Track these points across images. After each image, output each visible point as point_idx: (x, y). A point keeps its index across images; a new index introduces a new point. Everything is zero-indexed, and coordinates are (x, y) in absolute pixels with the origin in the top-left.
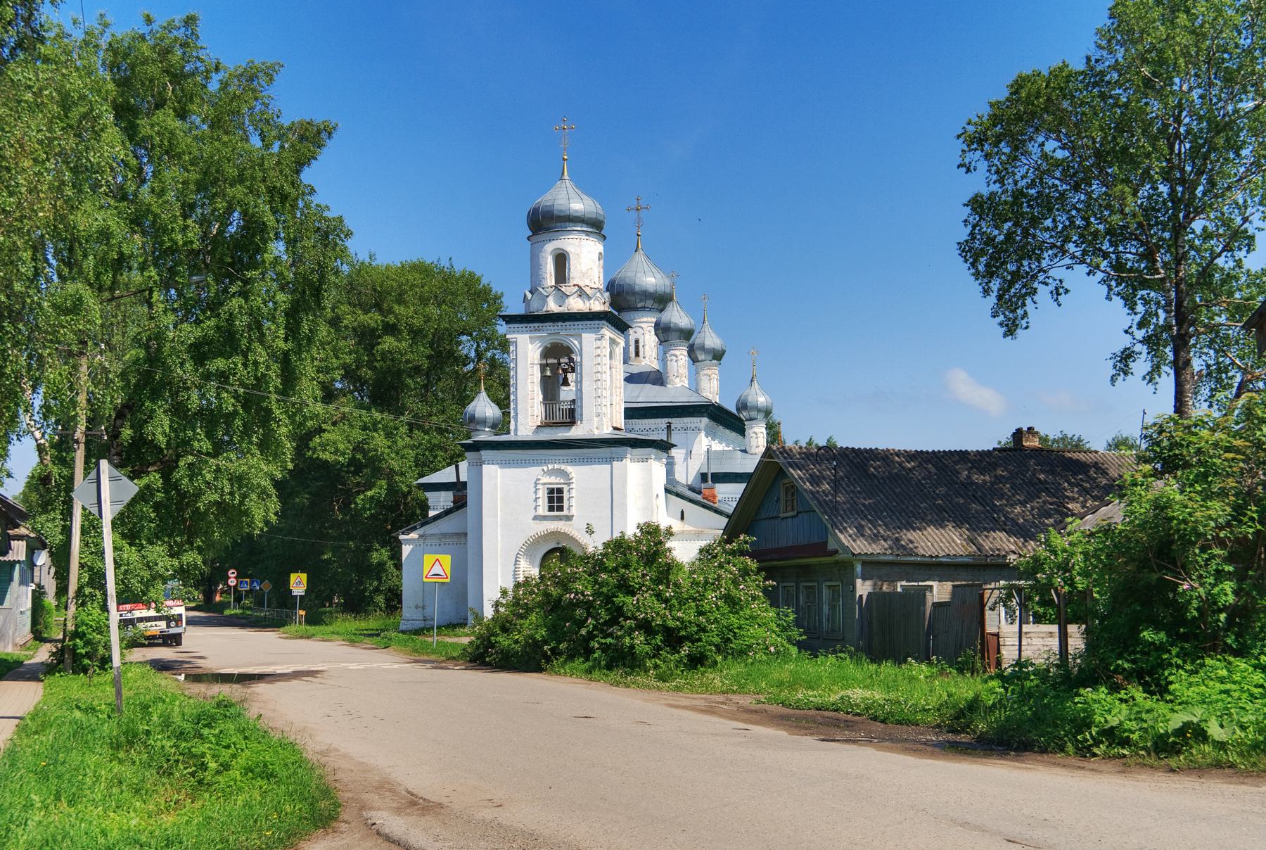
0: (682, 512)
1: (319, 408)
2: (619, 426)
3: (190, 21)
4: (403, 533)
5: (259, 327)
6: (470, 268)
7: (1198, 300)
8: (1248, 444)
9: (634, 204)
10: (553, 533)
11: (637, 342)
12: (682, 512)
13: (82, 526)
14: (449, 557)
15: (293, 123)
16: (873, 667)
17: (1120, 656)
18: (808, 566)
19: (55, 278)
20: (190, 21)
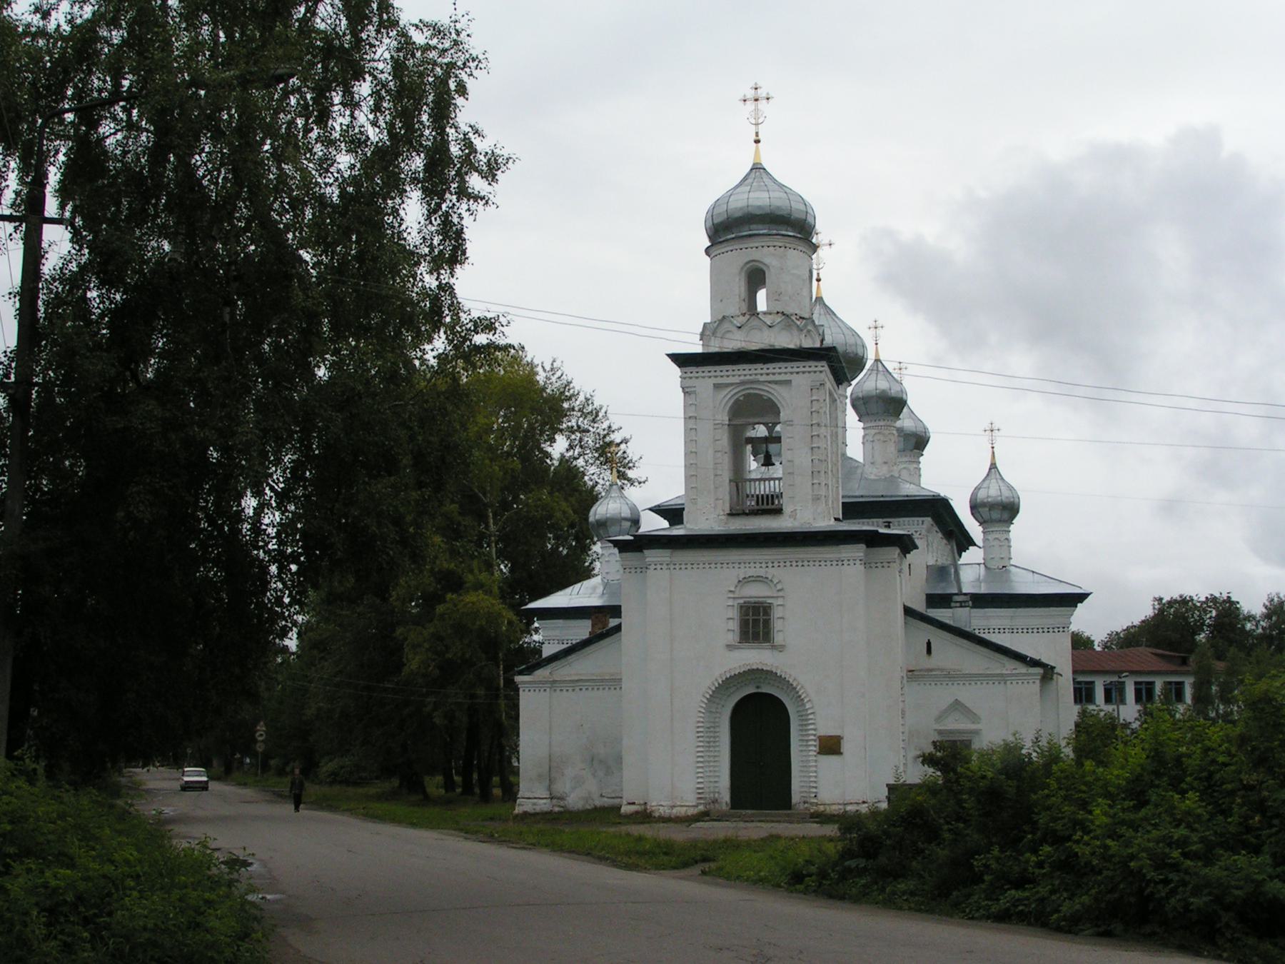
0: (929, 644)
1: (1112, 811)
2: (789, 452)
3: (467, 99)
4: (521, 673)
5: (555, 682)
6: (1219, 591)
7: (104, 332)
8: (795, 272)
9: (751, 94)
10: (752, 672)
11: (788, 382)
12: (929, 644)
13: (778, 837)
14: (611, 620)
15: (1207, 598)
16: (729, 834)
17: (273, 442)
18: (1086, 695)
19: (406, 461)
20: (467, 99)
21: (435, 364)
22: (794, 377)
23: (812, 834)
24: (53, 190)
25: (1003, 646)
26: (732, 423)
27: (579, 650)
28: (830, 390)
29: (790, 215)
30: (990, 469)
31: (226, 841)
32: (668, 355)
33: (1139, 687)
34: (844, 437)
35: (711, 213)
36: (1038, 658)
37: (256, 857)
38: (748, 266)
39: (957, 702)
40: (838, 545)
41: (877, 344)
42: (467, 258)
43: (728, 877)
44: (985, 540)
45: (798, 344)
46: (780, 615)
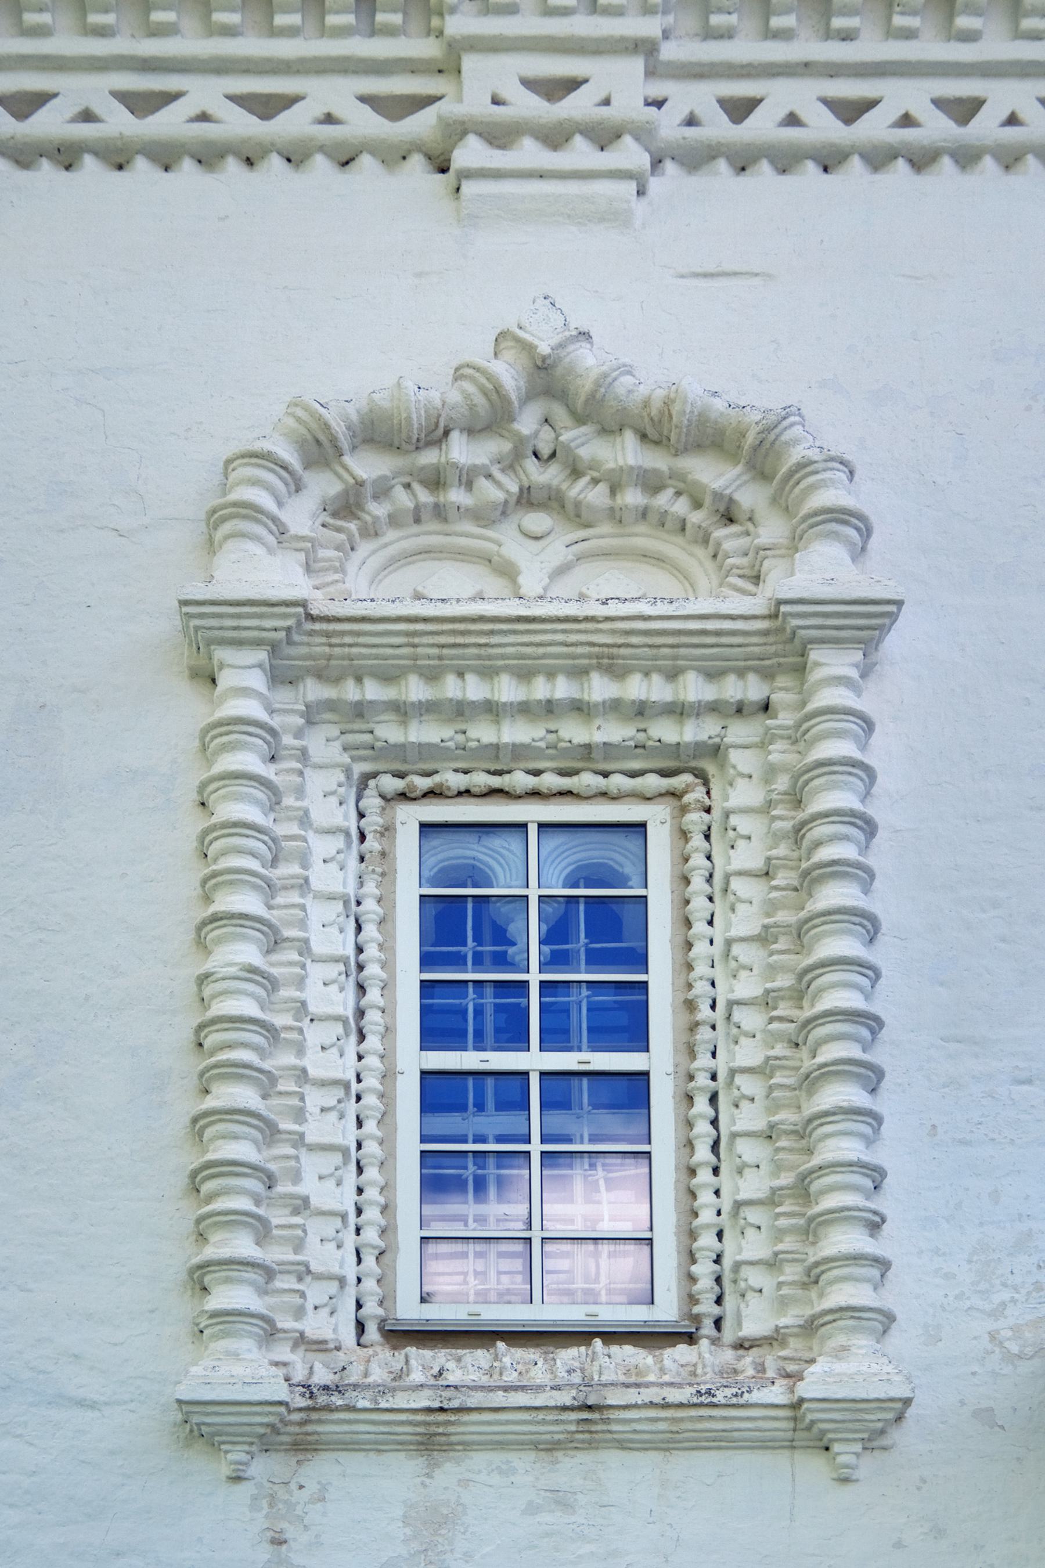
18: (475, 1031)
21: (673, 1369)
22: (466, 1317)
23: (246, 620)
24: (264, 1519)
25: (988, 62)
26: (289, 411)
27: (620, 171)
28: (239, 100)
29: (758, 948)
30: (900, 1400)
31: (680, 466)
32: (187, 92)
33: (581, 1020)
34: (676, 1194)
35: (871, 174)
36: (625, 1347)
37: (732, 852)
38: (441, 865)
39: (848, 121)
40: (283, 95)
41: (276, 630)
42: (444, 506)
43: (610, 14)
44: (769, 1031)
45: (637, 696)
46: (337, 1265)
